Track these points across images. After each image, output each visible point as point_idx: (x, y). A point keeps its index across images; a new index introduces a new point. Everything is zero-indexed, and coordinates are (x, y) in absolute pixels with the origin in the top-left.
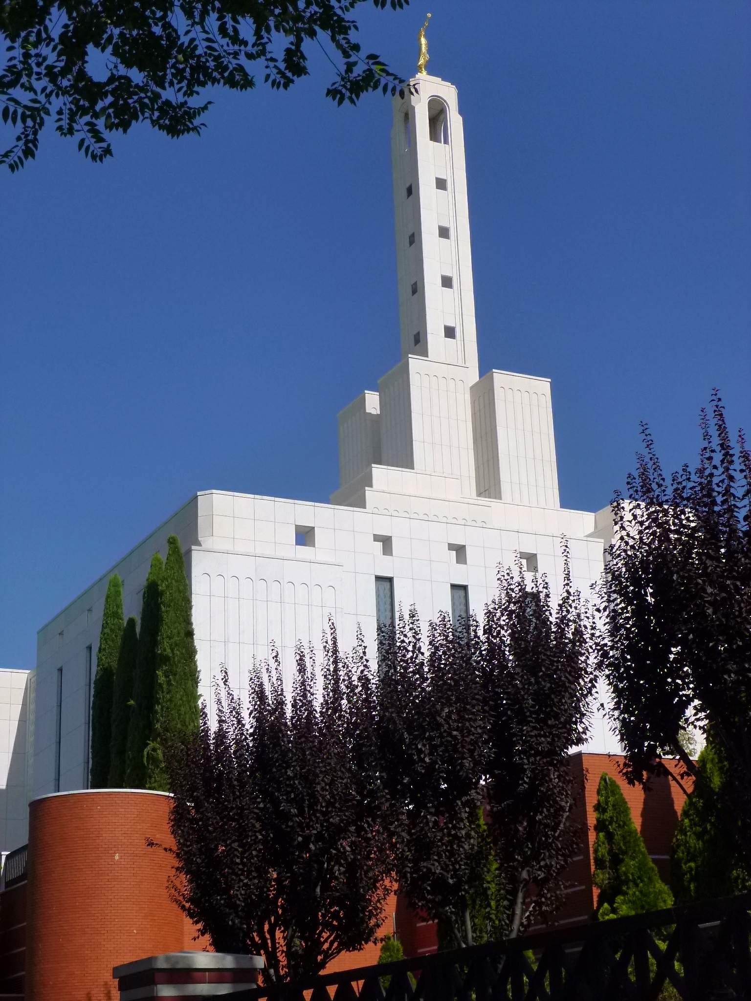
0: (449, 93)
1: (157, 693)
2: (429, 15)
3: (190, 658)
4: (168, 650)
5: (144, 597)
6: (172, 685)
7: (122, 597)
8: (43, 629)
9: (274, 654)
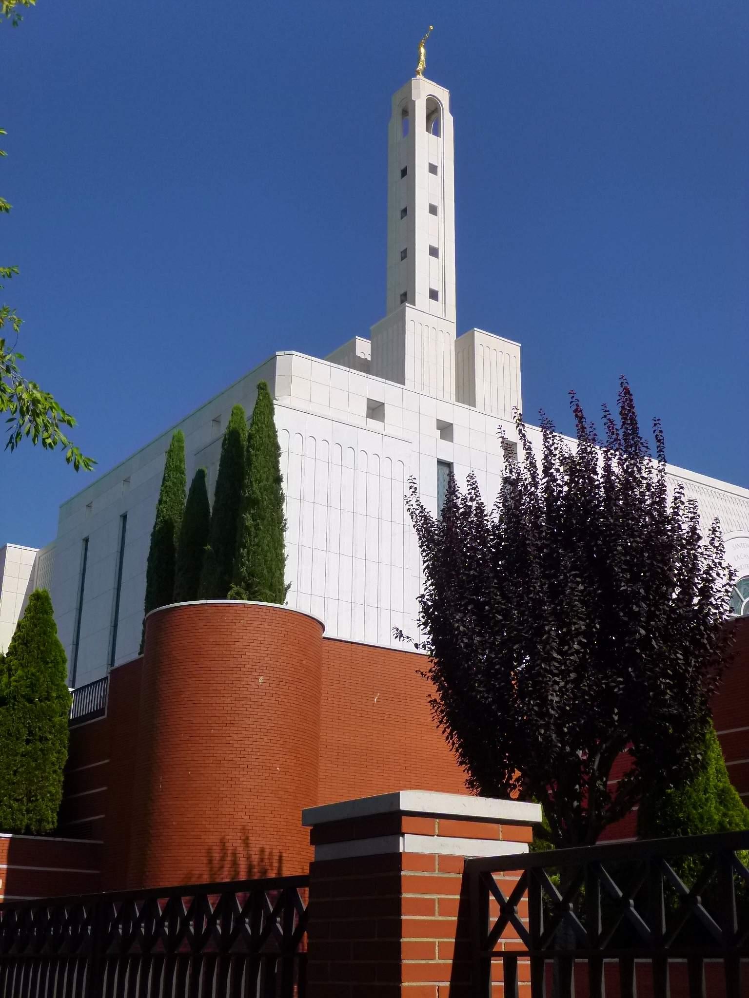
0: (443, 95)
1: (242, 536)
2: (431, 27)
3: (278, 504)
4: (258, 491)
5: (223, 444)
6: (259, 529)
7: (185, 453)
8: (67, 503)
9: (574, 408)
